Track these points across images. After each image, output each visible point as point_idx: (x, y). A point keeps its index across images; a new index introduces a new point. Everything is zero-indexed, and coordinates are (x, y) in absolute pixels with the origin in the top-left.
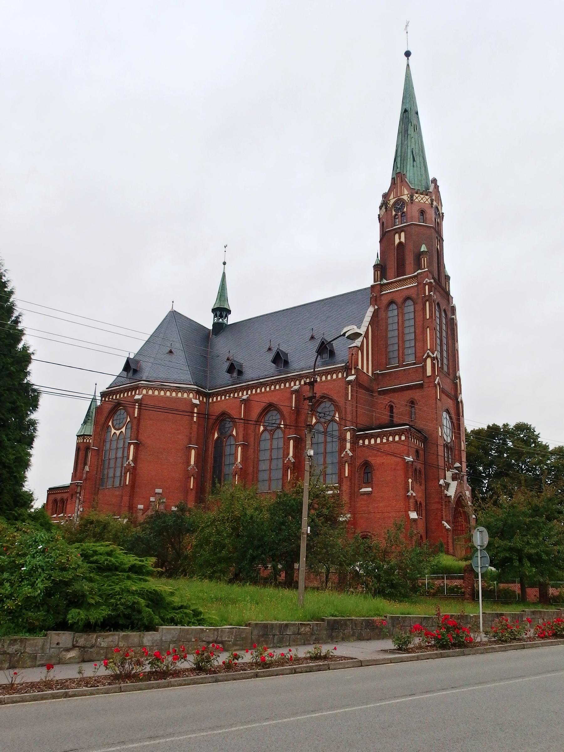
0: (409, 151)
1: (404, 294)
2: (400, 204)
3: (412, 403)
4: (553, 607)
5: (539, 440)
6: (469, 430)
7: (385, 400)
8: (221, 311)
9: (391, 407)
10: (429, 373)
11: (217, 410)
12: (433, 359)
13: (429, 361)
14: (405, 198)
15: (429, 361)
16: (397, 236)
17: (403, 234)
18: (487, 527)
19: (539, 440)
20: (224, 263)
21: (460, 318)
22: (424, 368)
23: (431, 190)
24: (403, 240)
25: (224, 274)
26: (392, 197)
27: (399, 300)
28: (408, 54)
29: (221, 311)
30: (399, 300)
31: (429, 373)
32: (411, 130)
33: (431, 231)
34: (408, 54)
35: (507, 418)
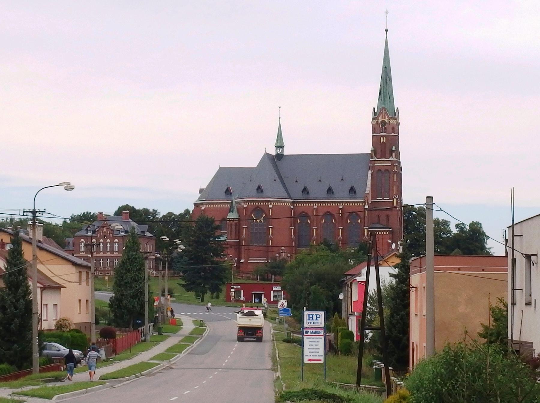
0: (387, 93)
2: (383, 123)
3: (388, 216)
4: (154, 265)
7: (377, 213)
8: (280, 146)
9: (379, 216)
10: (395, 204)
11: (300, 210)
12: (397, 199)
13: (395, 200)
14: (386, 121)
15: (395, 200)
16: (382, 138)
17: (385, 138)
20: (280, 118)
22: (393, 202)
23: (395, 115)
24: (385, 141)
25: (280, 124)
26: (380, 118)
27: (383, 170)
28: (387, 31)
29: (280, 146)
30: (383, 170)
31: (395, 204)
32: (388, 79)
34: (387, 31)
35: (406, 204)
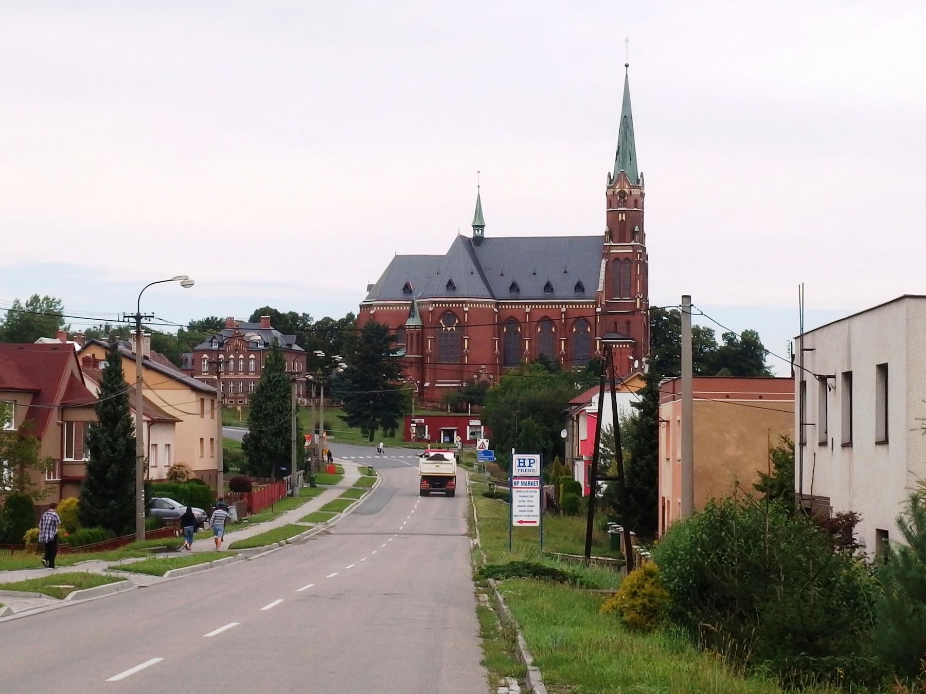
1: (625, 256)
2: (622, 194)
3: (628, 323)
5: (483, 657)
6: (651, 304)
7: (613, 318)
8: (479, 226)
10: (638, 306)
14: (626, 190)
18: (768, 377)
19: (483, 657)
21: (651, 262)
22: (636, 303)
23: (638, 183)
27: (622, 259)
28: (627, 66)
29: (479, 226)
30: (622, 259)
31: (638, 306)
32: (629, 133)
33: (637, 218)
34: (627, 66)
